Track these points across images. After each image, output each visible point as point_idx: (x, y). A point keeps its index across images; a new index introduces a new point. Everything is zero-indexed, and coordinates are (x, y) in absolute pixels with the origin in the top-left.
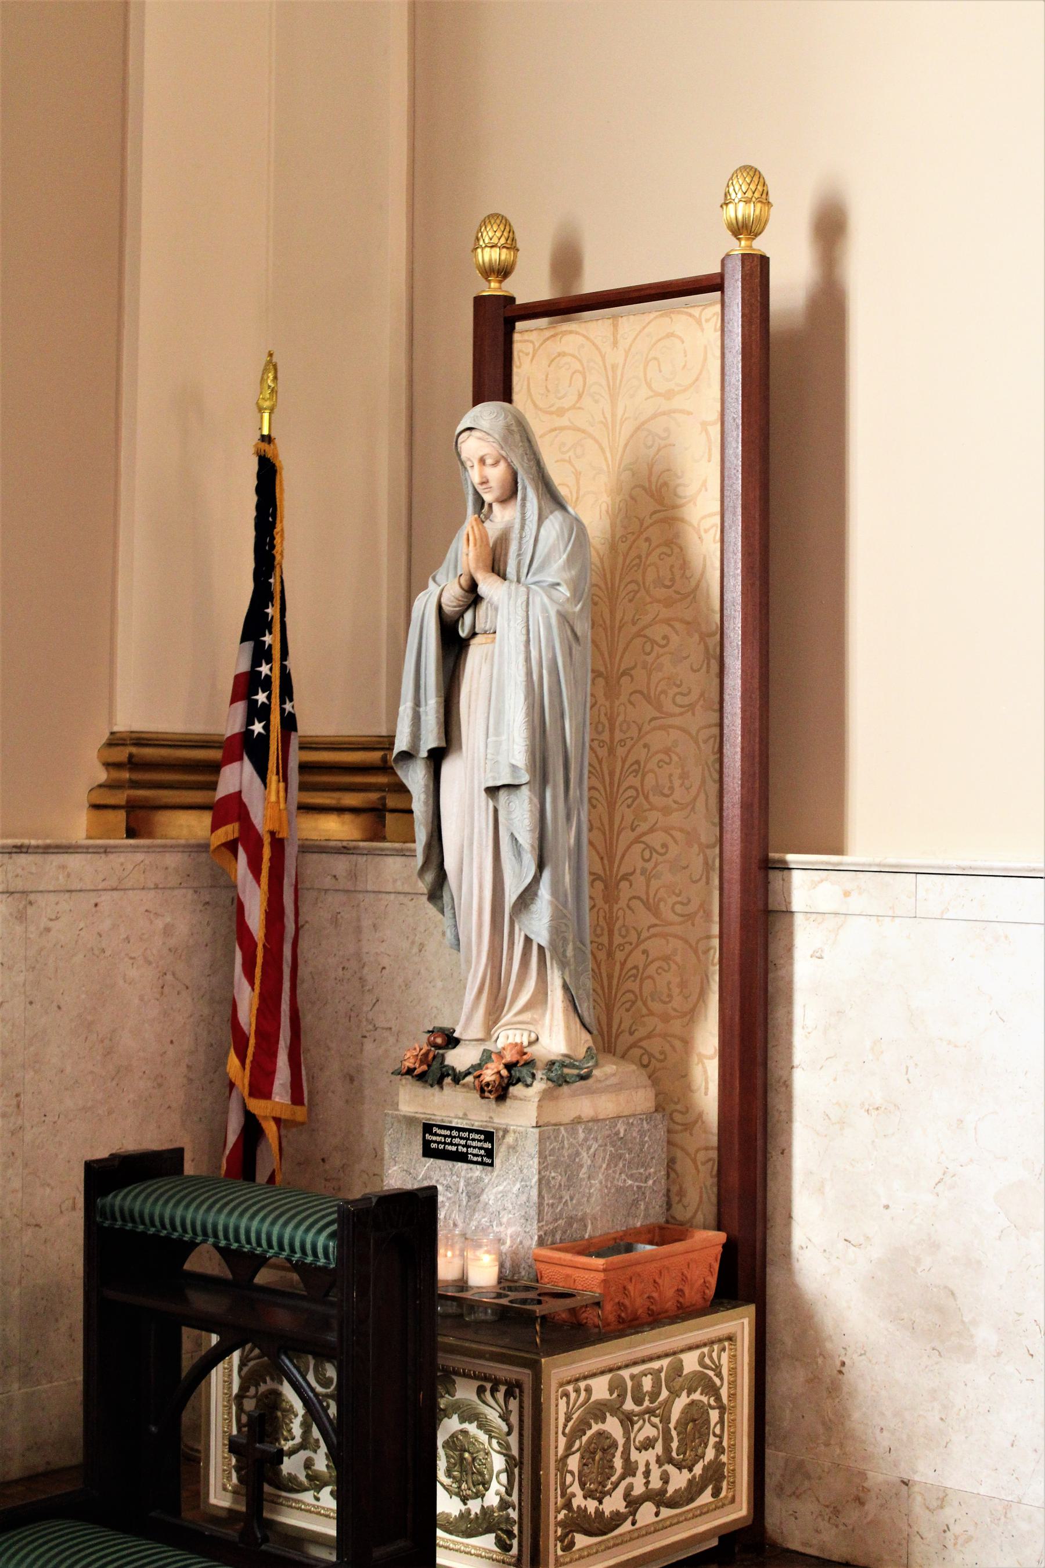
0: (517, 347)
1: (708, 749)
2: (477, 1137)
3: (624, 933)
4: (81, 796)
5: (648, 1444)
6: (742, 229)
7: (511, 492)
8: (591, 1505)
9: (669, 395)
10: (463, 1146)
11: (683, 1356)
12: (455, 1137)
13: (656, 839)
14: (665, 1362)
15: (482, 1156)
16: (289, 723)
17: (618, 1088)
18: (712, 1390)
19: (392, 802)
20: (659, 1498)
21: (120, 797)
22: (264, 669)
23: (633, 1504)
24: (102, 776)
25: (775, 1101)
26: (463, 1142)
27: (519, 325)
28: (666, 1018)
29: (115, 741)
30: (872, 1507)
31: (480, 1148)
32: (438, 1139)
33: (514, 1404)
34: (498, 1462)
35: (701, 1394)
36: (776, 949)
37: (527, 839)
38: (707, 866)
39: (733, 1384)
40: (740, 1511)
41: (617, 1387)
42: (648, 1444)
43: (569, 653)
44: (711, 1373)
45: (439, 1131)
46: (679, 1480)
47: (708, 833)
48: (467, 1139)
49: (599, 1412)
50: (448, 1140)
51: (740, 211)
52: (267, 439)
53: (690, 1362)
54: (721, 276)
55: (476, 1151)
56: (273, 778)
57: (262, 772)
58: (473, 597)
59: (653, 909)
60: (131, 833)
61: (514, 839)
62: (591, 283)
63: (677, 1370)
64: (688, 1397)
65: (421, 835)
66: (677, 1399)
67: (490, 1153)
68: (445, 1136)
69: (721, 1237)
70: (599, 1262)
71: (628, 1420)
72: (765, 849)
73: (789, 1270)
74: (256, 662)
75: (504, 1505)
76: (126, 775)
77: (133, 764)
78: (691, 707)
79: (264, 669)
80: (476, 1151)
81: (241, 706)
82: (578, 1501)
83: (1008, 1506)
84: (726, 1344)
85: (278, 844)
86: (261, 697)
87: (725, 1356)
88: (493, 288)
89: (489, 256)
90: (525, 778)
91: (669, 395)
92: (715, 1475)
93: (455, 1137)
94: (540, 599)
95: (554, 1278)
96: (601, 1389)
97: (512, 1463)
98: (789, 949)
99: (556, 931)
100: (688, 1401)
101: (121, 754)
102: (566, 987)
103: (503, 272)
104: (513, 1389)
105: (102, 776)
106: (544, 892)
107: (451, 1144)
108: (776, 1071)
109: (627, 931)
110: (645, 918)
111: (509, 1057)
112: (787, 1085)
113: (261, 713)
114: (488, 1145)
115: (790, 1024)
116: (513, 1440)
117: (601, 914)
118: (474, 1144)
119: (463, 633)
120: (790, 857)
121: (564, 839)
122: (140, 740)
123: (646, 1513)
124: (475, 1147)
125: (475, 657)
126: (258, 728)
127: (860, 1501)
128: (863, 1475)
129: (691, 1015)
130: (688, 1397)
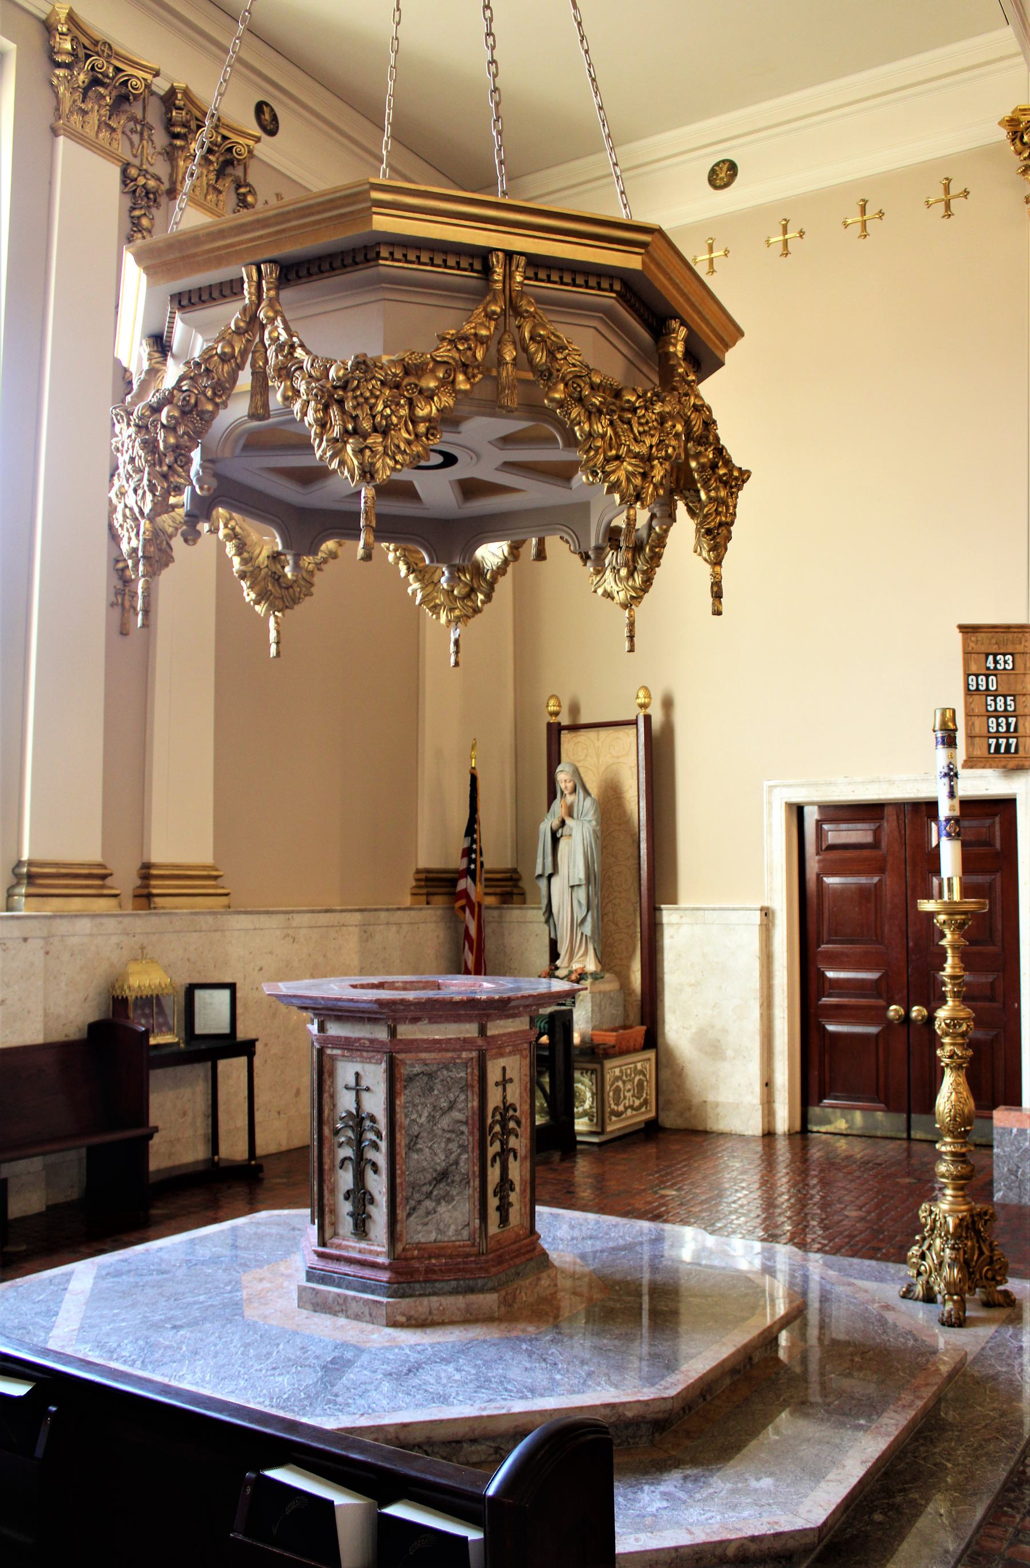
0: (562, 739)
1: (634, 872)
4: (408, 891)
5: (629, 1091)
6: (643, 706)
7: (574, 790)
8: (616, 1108)
9: (618, 757)
13: (616, 901)
14: (632, 1066)
16: (482, 864)
17: (610, 982)
18: (645, 1075)
19: (515, 891)
20: (632, 1107)
21: (424, 891)
22: (474, 846)
23: (626, 1108)
24: (414, 884)
25: (659, 985)
27: (563, 732)
28: (621, 959)
29: (418, 871)
30: (693, 1111)
33: (594, 1076)
34: (589, 1095)
36: (658, 935)
37: (584, 902)
38: (635, 910)
40: (653, 1114)
41: (621, 1071)
42: (629, 1091)
43: (596, 842)
46: (637, 1103)
47: (635, 898)
49: (617, 1079)
51: (641, 700)
52: (474, 768)
53: (639, 1066)
54: (637, 720)
56: (478, 883)
57: (474, 881)
58: (563, 823)
59: (616, 924)
60: (428, 903)
61: (579, 902)
62: (584, 719)
63: (636, 1067)
65: (545, 902)
67: (574, 1003)
69: (644, 1028)
70: (614, 1034)
71: (624, 1082)
72: (654, 903)
73: (664, 1037)
74: (472, 844)
75: (591, 1107)
76: (423, 883)
77: (427, 880)
78: (628, 858)
79: (474, 846)
81: (465, 860)
82: (613, 1106)
83: (738, 1105)
85: (480, 905)
86: (473, 856)
88: (553, 720)
89: (551, 709)
90: (584, 882)
91: (618, 757)
92: (646, 1102)
94: (587, 825)
95: (598, 1040)
96: (617, 1071)
97: (593, 1094)
98: (662, 935)
99: (593, 931)
101: (423, 876)
102: (595, 949)
103: (556, 714)
104: (593, 1071)
106: (589, 918)
108: (659, 975)
110: (613, 927)
111: (579, 971)
112: (662, 979)
113: (474, 861)
115: (662, 960)
116: (594, 1088)
119: (558, 836)
120: (663, 906)
121: (595, 902)
122: (428, 871)
123: (629, 1112)
125: (563, 844)
126: (473, 866)
127: (690, 1109)
128: (690, 1101)
129: (631, 957)
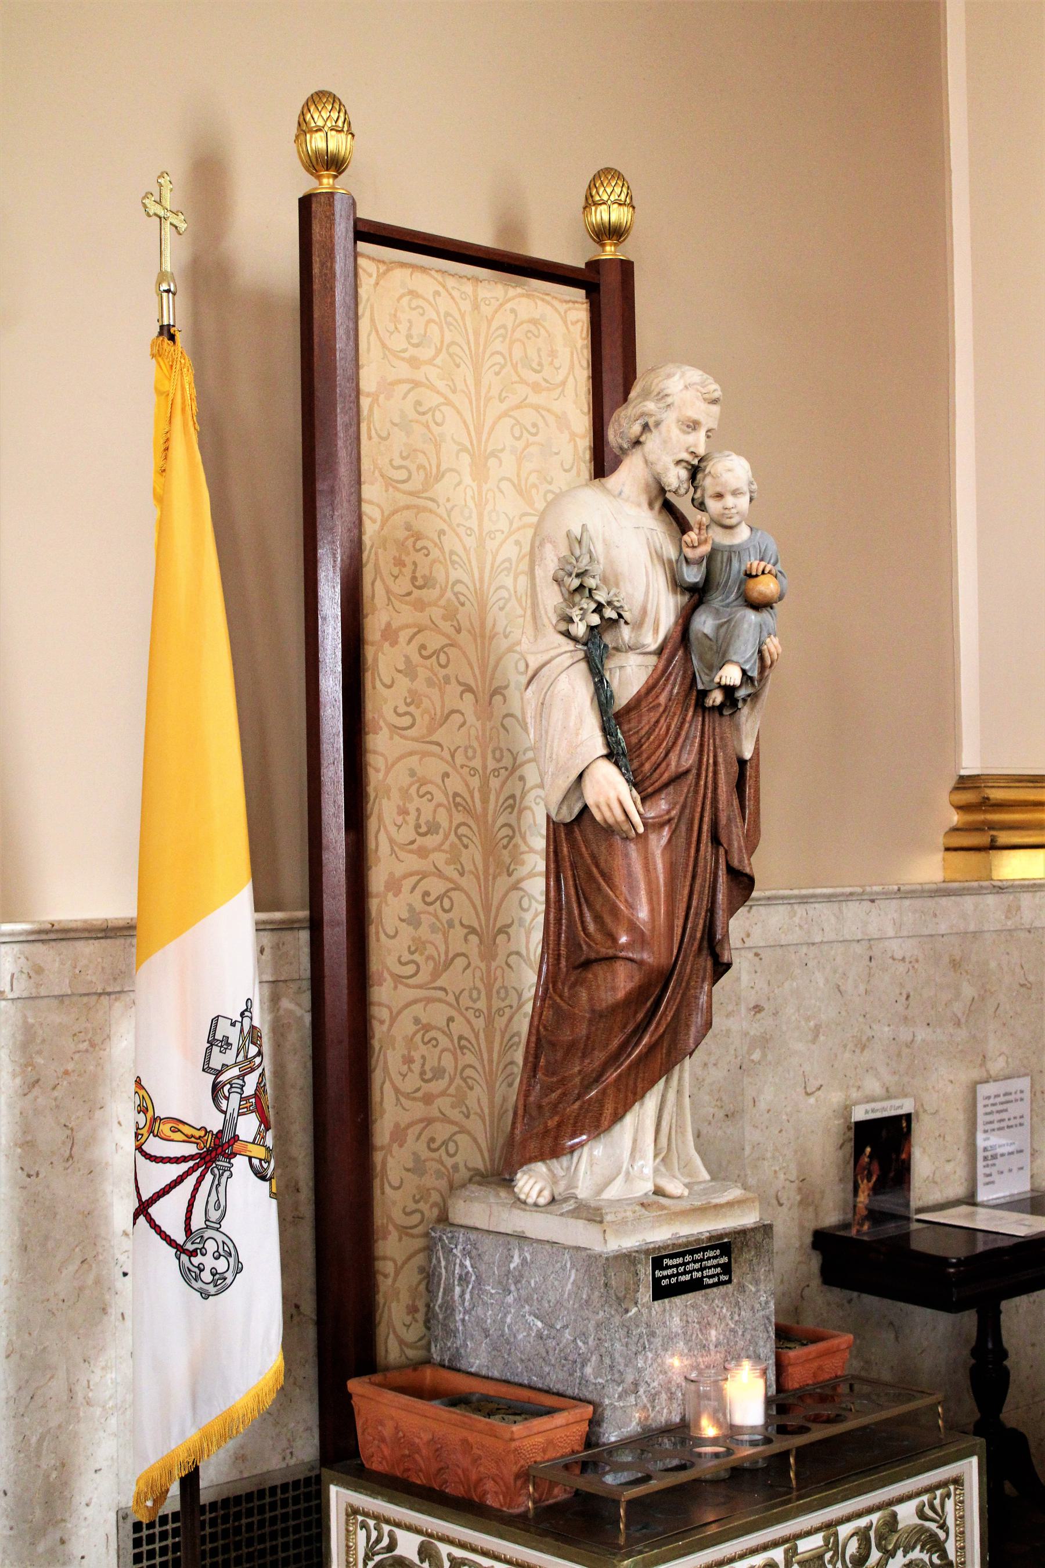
2: (711, 1254)
3: (503, 995)
10: (698, 1270)
11: (897, 1508)
12: (688, 1263)
14: (875, 1517)
15: (718, 1275)
24: (955, 818)
26: (697, 1266)
31: (715, 1267)
32: (669, 1272)
35: (921, 1551)
39: (961, 1535)
44: (933, 1526)
45: (670, 1262)
48: (702, 1260)
50: (681, 1269)
53: (906, 1513)
55: (711, 1272)
63: (892, 1522)
64: (904, 1556)
66: (891, 1560)
68: (677, 1266)
80: (711, 1272)
84: (952, 1488)
87: (950, 1504)
93: (688, 1263)
100: (906, 1561)
105: (955, 818)
107: (685, 1273)
109: (507, 992)
114: (724, 1260)
117: (478, 974)
118: (709, 1263)
124: (710, 1268)
130: (904, 1556)
